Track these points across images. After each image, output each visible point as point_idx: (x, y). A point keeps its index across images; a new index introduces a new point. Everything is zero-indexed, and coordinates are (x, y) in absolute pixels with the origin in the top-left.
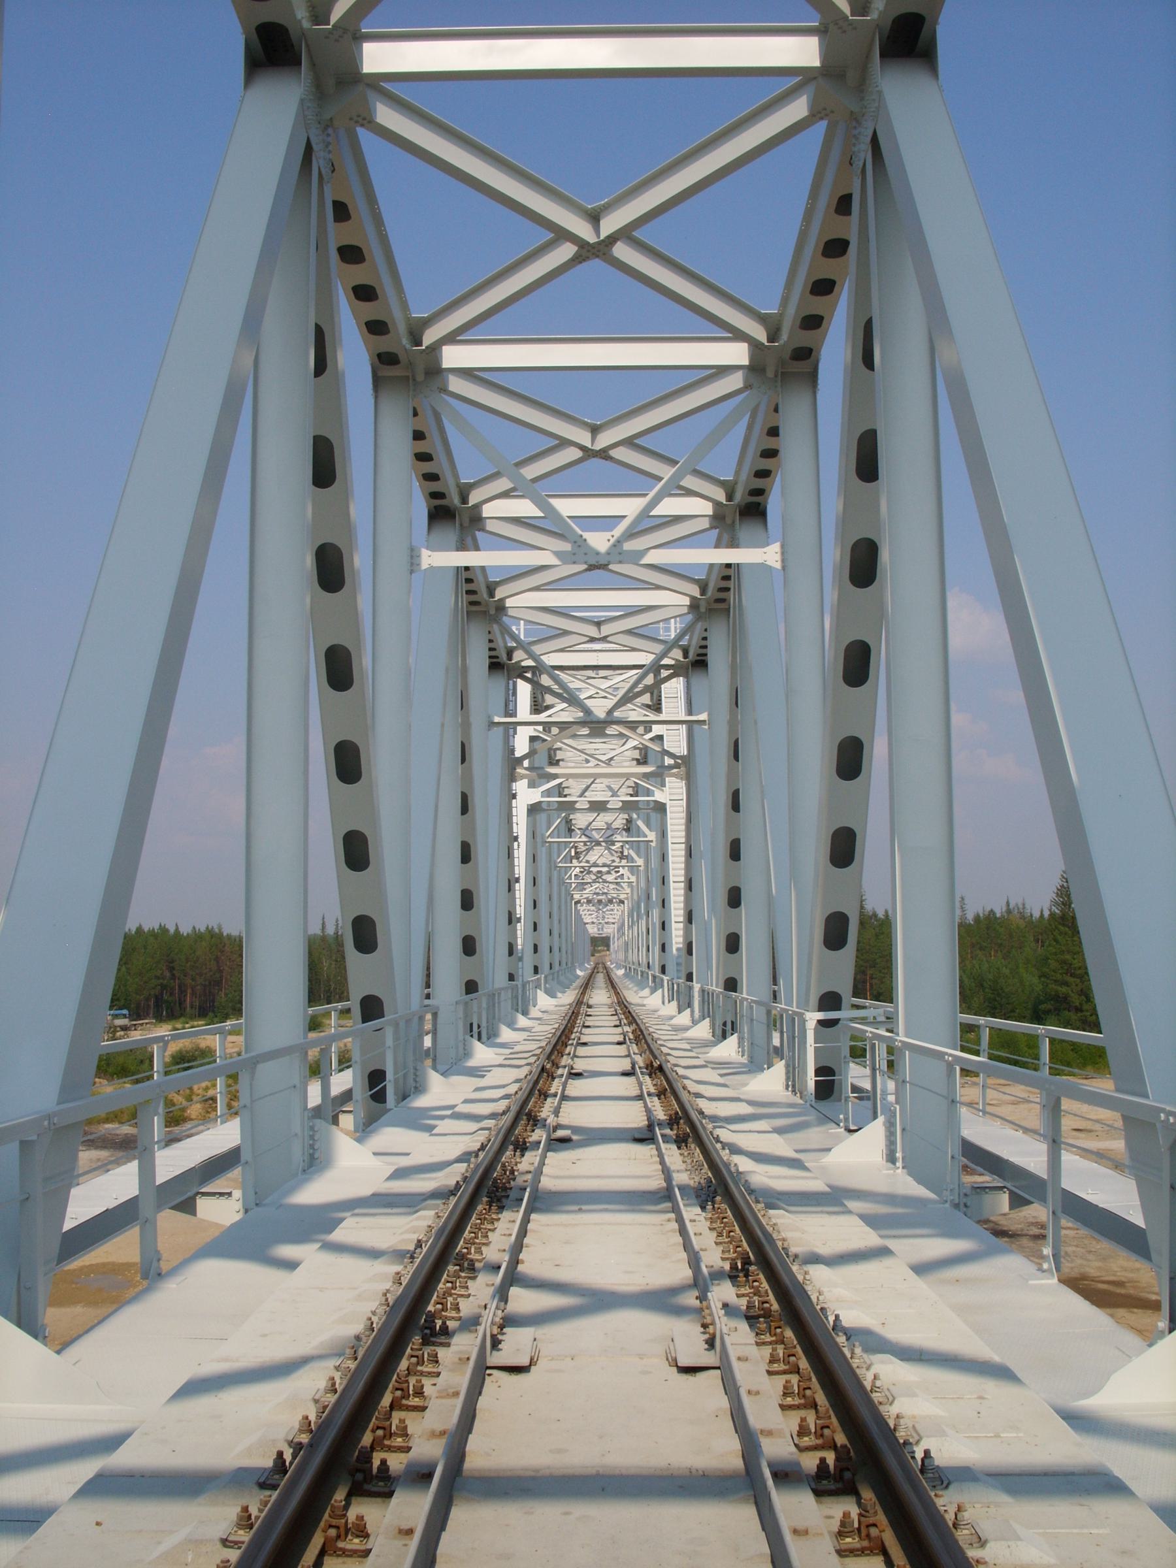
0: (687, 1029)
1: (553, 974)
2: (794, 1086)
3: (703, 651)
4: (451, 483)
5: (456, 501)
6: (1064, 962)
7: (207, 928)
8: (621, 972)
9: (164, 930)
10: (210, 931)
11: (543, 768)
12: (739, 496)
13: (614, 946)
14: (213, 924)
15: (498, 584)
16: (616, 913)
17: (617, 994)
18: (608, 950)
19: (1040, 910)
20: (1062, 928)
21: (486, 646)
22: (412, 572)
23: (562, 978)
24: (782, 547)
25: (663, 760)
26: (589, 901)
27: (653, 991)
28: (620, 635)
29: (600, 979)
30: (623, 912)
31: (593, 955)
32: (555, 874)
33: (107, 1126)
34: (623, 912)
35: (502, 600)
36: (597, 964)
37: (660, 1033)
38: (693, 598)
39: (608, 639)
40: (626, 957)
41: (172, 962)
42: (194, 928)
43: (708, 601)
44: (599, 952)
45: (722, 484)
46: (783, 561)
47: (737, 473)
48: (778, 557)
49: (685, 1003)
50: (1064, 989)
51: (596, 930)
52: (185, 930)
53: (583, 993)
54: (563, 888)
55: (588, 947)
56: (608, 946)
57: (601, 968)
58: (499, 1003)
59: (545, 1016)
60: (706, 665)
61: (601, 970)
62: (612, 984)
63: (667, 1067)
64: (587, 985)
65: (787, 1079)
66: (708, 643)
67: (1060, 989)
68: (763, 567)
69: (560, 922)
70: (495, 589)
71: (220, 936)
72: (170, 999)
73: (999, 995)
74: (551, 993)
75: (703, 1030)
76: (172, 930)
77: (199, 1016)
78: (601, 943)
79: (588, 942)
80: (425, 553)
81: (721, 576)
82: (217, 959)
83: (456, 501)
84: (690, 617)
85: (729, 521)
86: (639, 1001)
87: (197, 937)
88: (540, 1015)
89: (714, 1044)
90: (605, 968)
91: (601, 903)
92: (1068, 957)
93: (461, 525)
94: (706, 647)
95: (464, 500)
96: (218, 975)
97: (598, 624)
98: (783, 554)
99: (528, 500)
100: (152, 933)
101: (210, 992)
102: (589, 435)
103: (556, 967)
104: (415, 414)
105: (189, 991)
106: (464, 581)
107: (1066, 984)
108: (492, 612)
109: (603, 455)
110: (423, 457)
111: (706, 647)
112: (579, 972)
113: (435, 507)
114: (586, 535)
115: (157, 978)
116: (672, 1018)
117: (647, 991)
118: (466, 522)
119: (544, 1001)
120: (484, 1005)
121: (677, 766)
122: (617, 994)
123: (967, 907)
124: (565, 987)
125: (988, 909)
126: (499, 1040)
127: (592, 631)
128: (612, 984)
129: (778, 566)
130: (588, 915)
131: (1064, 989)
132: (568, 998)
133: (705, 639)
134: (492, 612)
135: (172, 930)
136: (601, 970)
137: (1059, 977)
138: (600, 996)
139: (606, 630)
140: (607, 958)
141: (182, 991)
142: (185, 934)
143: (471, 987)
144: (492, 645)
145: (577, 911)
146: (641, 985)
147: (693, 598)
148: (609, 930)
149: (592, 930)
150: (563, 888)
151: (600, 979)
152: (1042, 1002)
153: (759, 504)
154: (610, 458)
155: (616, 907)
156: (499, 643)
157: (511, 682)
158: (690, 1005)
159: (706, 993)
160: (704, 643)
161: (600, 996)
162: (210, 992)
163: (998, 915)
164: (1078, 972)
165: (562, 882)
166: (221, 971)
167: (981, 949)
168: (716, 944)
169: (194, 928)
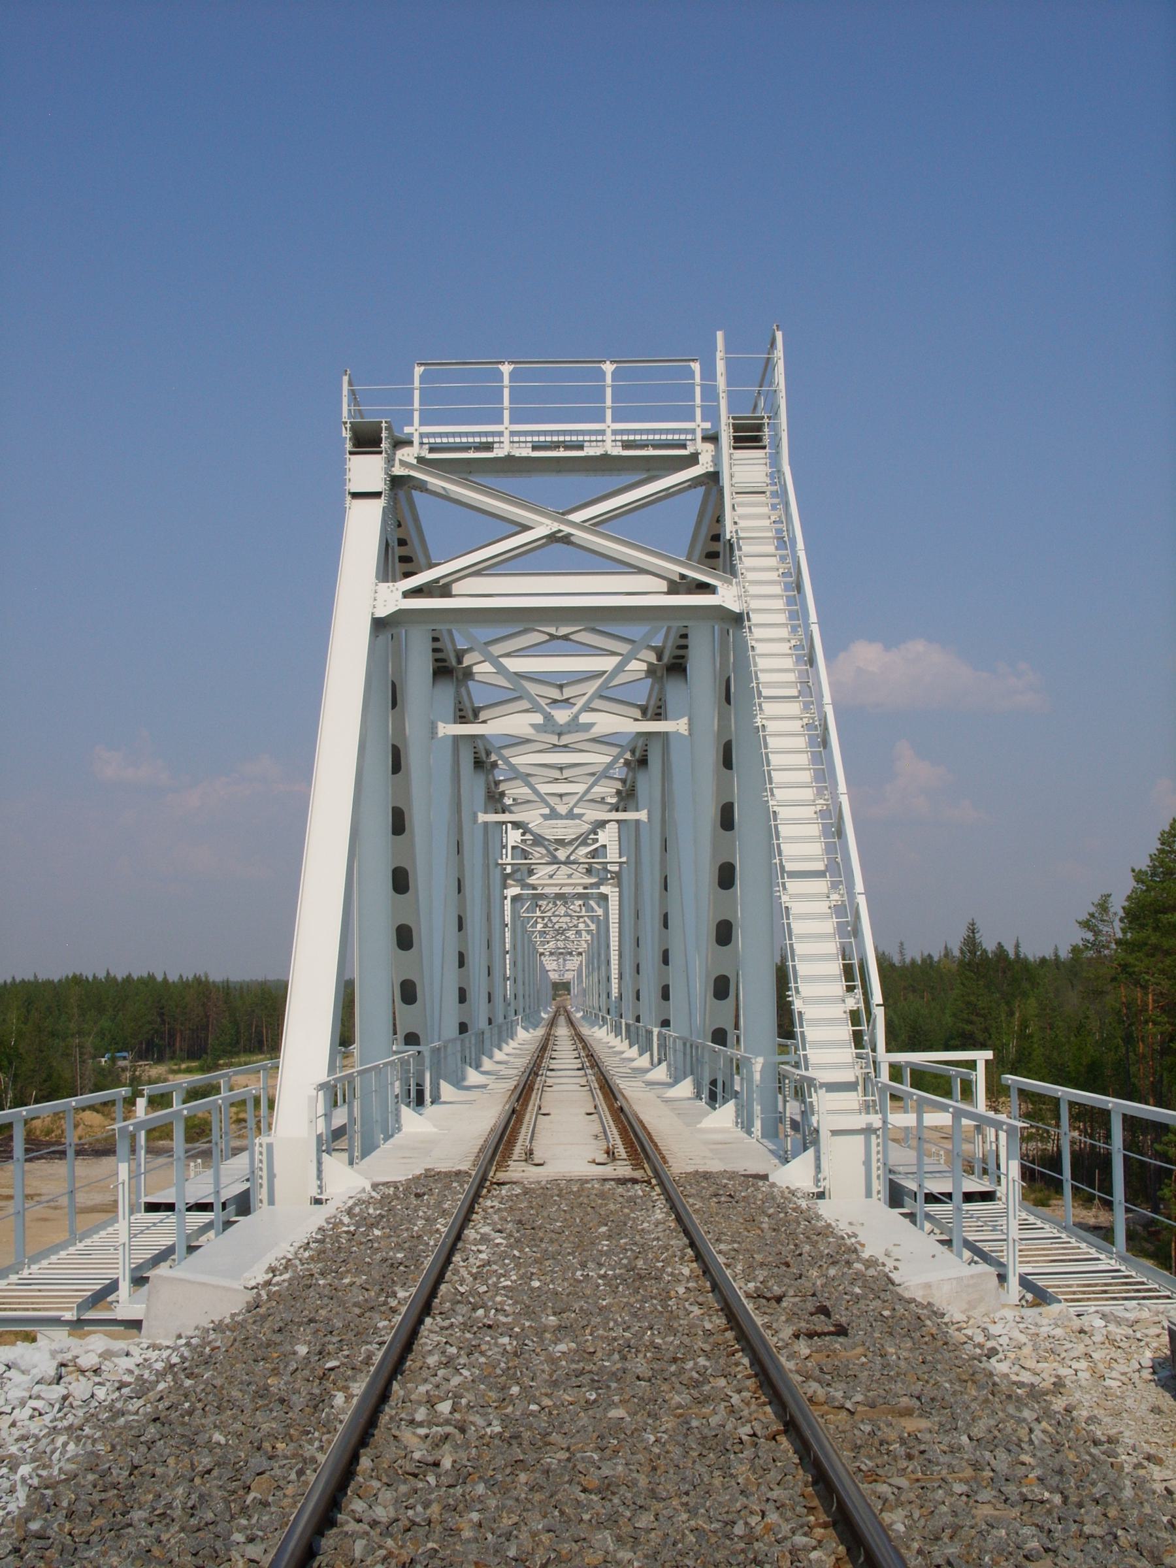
0: (647, 1071)
1: (507, 1023)
2: (742, 1123)
3: (681, 652)
4: (449, 647)
5: (454, 662)
6: (969, 1003)
7: (195, 976)
8: (579, 1015)
9: (152, 977)
10: (198, 980)
11: (523, 880)
12: (666, 659)
13: (575, 990)
14: (201, 973)
15: (481, 709)
16: (574, 963)
17: (575, 1029)
18: (569, 994)
19: (1054, 947)
20: (968, 973)
21: (429, 645)
22: (432, 738)
23: (532, 1020)
24: (690, 720)
25: (443, 1400)
26: (551, 954)
27: (601, 1027)
28: (583, 633)
29: (562, 1020)
30: (581, 962)
31: (554, 999)
32: (519, 923)
33: (161, 1142)
34: (581, 962)
35: (470, 667)
36: (558, 1008)
37: (610, 1064)
38: (650, 664)
39: (571, 701)
40: (584, 1001)
41: (162, 1008)
42: (181, 976)
43: (627, 791)
44: (560, 996)
45: (639, 706)
46: (690, 730)
47: (665, 642)
48: (686, 727)
49: (618, 1033)
50: (968, 1028)
51: (557, 976)
52: (173, 977)
53: (550, 1029)
54: (526, 936)
55: (550, 992)
56: (569, 990)
57: (562, 1012)
58: (445, 1058)
59: (511, 1059)
60: (684, 670)
61: (562, 1012)
62: (571, 1023)
63: (594, 1054)
64: (552, 1023)
65: (737, 1116)
66: (648, 748)
67: (966, 1027)
68: (677, 733)
69: (524, 971)
70: (463, 656)
71: (207, 982)
72: (161, 1043)
73: (918, 1033)
74: (526, 1029)
75: (661, 1073)
76: (160, 978)
77: (188, 1058)
78: (561, 988)
79: (550, 987)
80: (441, 725)
81: (705, 552)
82: (204, 1005)
83: (454, 662)
84: (650, 681)
85: (659, 674)
86: (590, 1033)
87: (185, 985)
88: (505, 1058)
89: (671, 1085)
90: (566, 1011)
91: (562, 954)
92: (972, 998)
93: (457, 678)
94: (685, 647)
95: (460, 661)
96: (205, 1020)
97: (561, 769)
98: (689, 725)
99: (512, 670)
100: (141, 981)
101: (198, 1037)
102: (556, 737)
103: (527, 1011)
104: (399, 525)
105: (179, 1035)
106: (397, 560)
107: (971, 1022)
108: (497, 796)
109: (565, 540)
110: (461, 710)
111: (683, 657)
112: (543, 1015)
113: (438, 667)
114: (553, 712)
115: (150, 1023)
116: (633, 1060)
117: (596, 1028)
118: (461, 677)
119: (522, 1034)
120: (473, 1041)
121: (612, 878)
122: (575, 1029)
123: (905, 952)
124: (535, 1027)
125: (926, 954)
126: (466, 1083)
127: (555, 694)
128: (571, 1023)
129: (686, 733)
130: (550, 964)
131: (968, 1028)
132: (540, 1032)
133: (660, 707)
134: (497, 796)
135: (160, 978)
136: (562, 1012)
137: (966, 1016)
138: (562, 1031)
139: (568, 692)
140: (568, 1002)
141: (172, 1036)
142: (90, 979)
143: (463, 1028)
144: (437, 645)
145: (541, 962)
146: (592, 1025)
147: (650, 664)
148: (568, 976)
149: (554, 976)
150: (519, 923)
151: (562, 1020)
152: (952, 1038)
153: (681, 664)
154: (570, 640)
155: (576, 958)
156: (446, 644)
157: (463, 690)
158: (621, 1034)
159: (688, 1045)
160: (683, 642)
161: (562, 1031)
162: (198, 1037)
163: (936, 959)
164: (982, 1012)
165: (530, 941)
166: (207, 1017)
167: (914, 991)
168: (701, 987)
169: (181, 976)
